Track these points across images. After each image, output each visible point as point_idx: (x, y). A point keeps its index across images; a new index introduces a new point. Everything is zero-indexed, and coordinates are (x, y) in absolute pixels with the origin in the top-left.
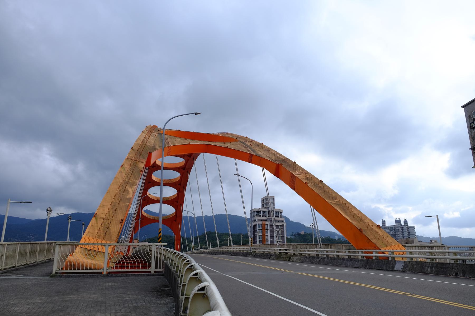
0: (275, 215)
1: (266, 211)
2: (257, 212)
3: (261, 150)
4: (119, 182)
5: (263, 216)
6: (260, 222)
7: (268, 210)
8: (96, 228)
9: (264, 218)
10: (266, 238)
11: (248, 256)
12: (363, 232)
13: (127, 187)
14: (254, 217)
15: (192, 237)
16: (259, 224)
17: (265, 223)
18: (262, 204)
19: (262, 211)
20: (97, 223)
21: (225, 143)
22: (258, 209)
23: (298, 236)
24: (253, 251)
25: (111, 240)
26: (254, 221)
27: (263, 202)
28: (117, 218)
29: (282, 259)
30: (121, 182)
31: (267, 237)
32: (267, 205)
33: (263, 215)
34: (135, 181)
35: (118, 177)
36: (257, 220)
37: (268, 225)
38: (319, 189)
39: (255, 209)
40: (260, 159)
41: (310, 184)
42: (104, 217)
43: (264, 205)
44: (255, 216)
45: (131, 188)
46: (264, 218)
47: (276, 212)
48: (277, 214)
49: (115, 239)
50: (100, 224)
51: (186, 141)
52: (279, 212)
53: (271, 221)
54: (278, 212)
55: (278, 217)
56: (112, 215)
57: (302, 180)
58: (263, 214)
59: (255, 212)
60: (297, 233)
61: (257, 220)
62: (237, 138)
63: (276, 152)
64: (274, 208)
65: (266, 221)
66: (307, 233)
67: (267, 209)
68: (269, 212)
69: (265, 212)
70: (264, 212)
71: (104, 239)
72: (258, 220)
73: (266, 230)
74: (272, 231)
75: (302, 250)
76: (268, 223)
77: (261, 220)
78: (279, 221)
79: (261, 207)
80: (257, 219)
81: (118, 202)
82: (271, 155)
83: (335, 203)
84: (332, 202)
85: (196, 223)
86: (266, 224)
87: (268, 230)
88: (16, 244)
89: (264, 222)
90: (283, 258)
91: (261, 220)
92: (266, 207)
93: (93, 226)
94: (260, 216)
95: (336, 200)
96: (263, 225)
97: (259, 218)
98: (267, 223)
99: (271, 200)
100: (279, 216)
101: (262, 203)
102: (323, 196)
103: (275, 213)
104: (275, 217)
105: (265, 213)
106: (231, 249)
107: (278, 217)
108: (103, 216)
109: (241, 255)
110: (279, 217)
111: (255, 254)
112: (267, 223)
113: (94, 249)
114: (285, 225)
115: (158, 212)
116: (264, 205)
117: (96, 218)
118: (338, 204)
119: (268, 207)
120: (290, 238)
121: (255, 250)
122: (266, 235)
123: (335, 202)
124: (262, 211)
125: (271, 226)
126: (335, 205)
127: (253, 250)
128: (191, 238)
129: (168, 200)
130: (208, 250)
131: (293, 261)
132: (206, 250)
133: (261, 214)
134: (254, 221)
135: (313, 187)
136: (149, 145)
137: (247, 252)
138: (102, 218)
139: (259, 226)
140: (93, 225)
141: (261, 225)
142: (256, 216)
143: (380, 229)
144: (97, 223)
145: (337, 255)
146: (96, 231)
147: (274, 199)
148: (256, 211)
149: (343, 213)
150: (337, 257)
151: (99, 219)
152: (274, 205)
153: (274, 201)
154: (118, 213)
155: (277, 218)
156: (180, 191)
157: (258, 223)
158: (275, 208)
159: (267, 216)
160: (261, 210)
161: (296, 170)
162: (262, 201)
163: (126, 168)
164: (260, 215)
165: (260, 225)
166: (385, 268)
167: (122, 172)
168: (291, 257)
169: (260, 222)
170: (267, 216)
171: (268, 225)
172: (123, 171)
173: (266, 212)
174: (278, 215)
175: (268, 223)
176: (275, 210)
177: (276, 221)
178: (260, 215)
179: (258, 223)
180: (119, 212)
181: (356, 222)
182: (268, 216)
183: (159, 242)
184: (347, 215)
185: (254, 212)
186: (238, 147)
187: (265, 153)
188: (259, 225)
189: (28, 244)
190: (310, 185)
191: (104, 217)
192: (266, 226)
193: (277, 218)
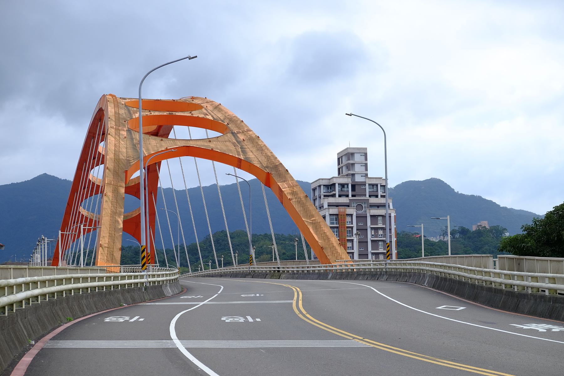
0: (369, 192)
1: (348, 185)
2: (327, 186)
3: (254, 150)
4: (109, 213)
5: (340, 196)
6: (334, 211)
7: (353, 180)
8: (104, 255)
9: (344, 200)
10: (348, 246)
11: (247, 277)
12: (323, 250)
13: (117, 217)
14: (320, 197)
15: (176, 247)
16: (330, 215)
17: (345, 212)
18: (341, 165)
19: (339, 184)
20: (104, 251)
21: (210, 141)
22: (330, 179)
23: (461, 236)
24: (252, 271)
25: (117, 263)
26: (320, 208)
27: (342, 163)
28: (116, 246)
29: (275, 277)
30: (110, 212)
31: (351, 243)
32: (349, 170)
33: (342, 193)
34: (121, 210)
35: (107, 208)
36: (326, 206)
37: (351, 215)
38: (301, 206)
39: (322, 179)
40: (250, 165)
41: (293, 200)
42: (107, 246)
43: (344, 168)
44: (322, 197)
45: (120, 218)
46: (344, 200)
47: (372, 185)
48: (375, 189)
49: (120, 262)
50: (106, 252)
51: (162, 142)
52: (379, 186)
53: (359, 207)
54: (377, 185)
55: (377, 196)
56: (113, 244)
57: (287, 195)
58: (342, 191)
59: (322, 187)
60: (457, 228)
61: (326, 206)
62: (228, 124)
63: (272, 152)
64: (367, 175)
65: (348, 206)
66: (486, 229)
67: (350, 180)
68: (353, 187)
69: (346, 186)
70: (342, 186)
71: (112, 263)
72: (328, 206)
73: (348, 227)
74: (362, 230)
75: (558, 278)
76: (352, 211)
77: (337, 206)
78: (378, 206)
79: (337, 175)
80: (326, 202)
81: (113, 232)
82: (263, 158)
83: (310, 221)
84: (308, 221)
85: (182, 229)
86: (347, 215)
87: (352, 228)
88: (23, 268)
89: (342, 209)
90: (275, 276)
91: (337, 205)
92: (347, 175)
93: (102, 254)
94: (334, 196)
95: (313, 219)
96: (340, 217)
97: (331, 200)
98: (349, 211)
99: (358, 158)
100: (380, 193)
101: (339, 164)
102: (301, 215)
103: (369, 188)
104: (370, 196)
105: (345, 189)
106: (233, 269)
107: (377, 196)
108: (107, 245)
109: (240, 277)
110: (379, 196)
111: (254, 274)
112: (349, 211)
113: (108, 270)
114: (393, 215)
115: (70, 180)
116: (344, 168)
117: (102, 248)
118: (312, 223)
119: (353, 175)
120: (440, 241)
121: (253, 270)
122: (348, 240)
123: (311, 220)
124: (339, 184)
125: (361, 218)
126: (309, 224)
127: (251, 270)
128: (173, 250)
129: (129, 186)
130: (200, 273)
131: (281, 279)
132: (199, 274)
133: (335, 190)
134: (320, 208)
135: (296, 205)
136: (123, 159)
137: (239, 272)
138: (106, 247)
139: (331, 219)
140: (102, 252)
141: (336, 217)
142: (325, 196)
143: (340, 247)
144: (104, 251)
145: (318, 270)
146: (106, 258)
147: (366, 155)
148: (324, 185)
149: (314, 232)
150: (307, 272)
151: (104, 248)
152: (366, 170)
153: (366, 159)
154: (116, 242)
155: (373, 200)
156: (150, 170)
157: (329, 212)
158: (369, 176)
159: (350, 196)
160: (335, 181)
161: (284, 181)
162: (339, 159)
163: (109, 196)
164: (334, 192)
165: (335, 217)
166: (324, 279)
167: (107, 202)
168: (281, 275)
169: (334, 211)
170: (350, 196)
171: (351, 215)
172: (108, 200)
173: (348, 187)
174: (377, 191)
175: (352, 211)
176: (368, 182)
177: (373, 206)
178: (334, 192)
179: (329, 212)
180: (117, 241)
181: (322, 241)
182: (353, 196)
183: (149, 264)
184: (316, 234)
185: (320, 186)
186: (227, 146)
187: (257, 156)
188: (332, 217)
189: (40, 270)
190: (293, 202)
191: (107, 246)
192: (348, 219)
193: (373, 200)
